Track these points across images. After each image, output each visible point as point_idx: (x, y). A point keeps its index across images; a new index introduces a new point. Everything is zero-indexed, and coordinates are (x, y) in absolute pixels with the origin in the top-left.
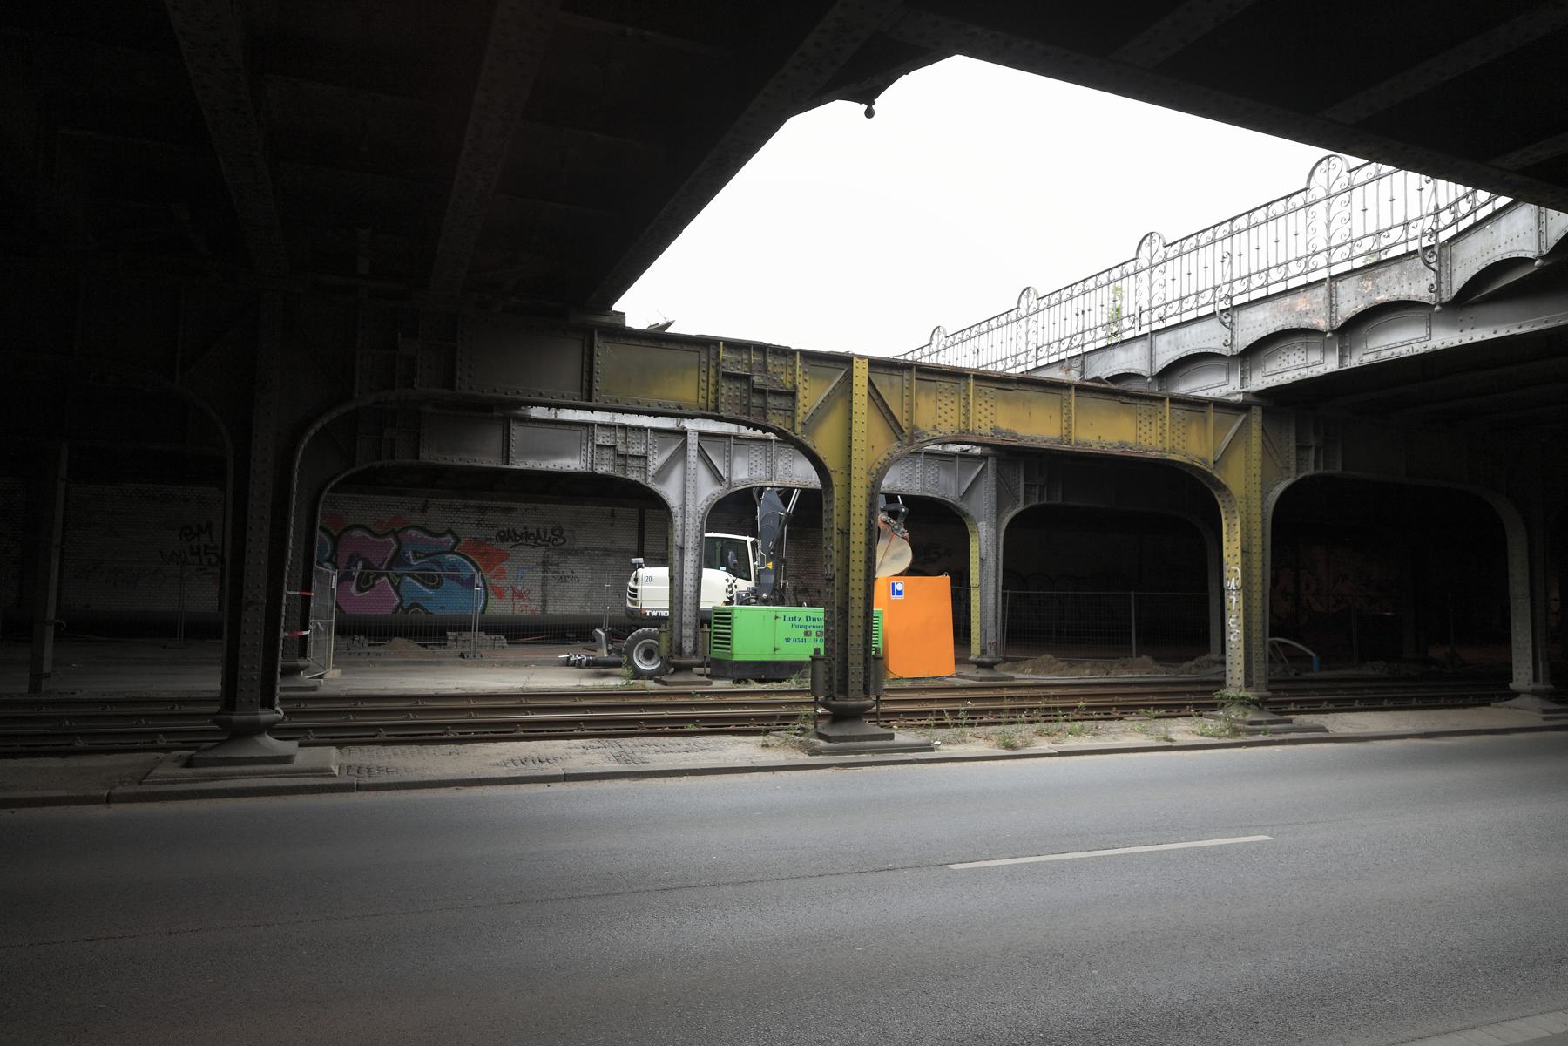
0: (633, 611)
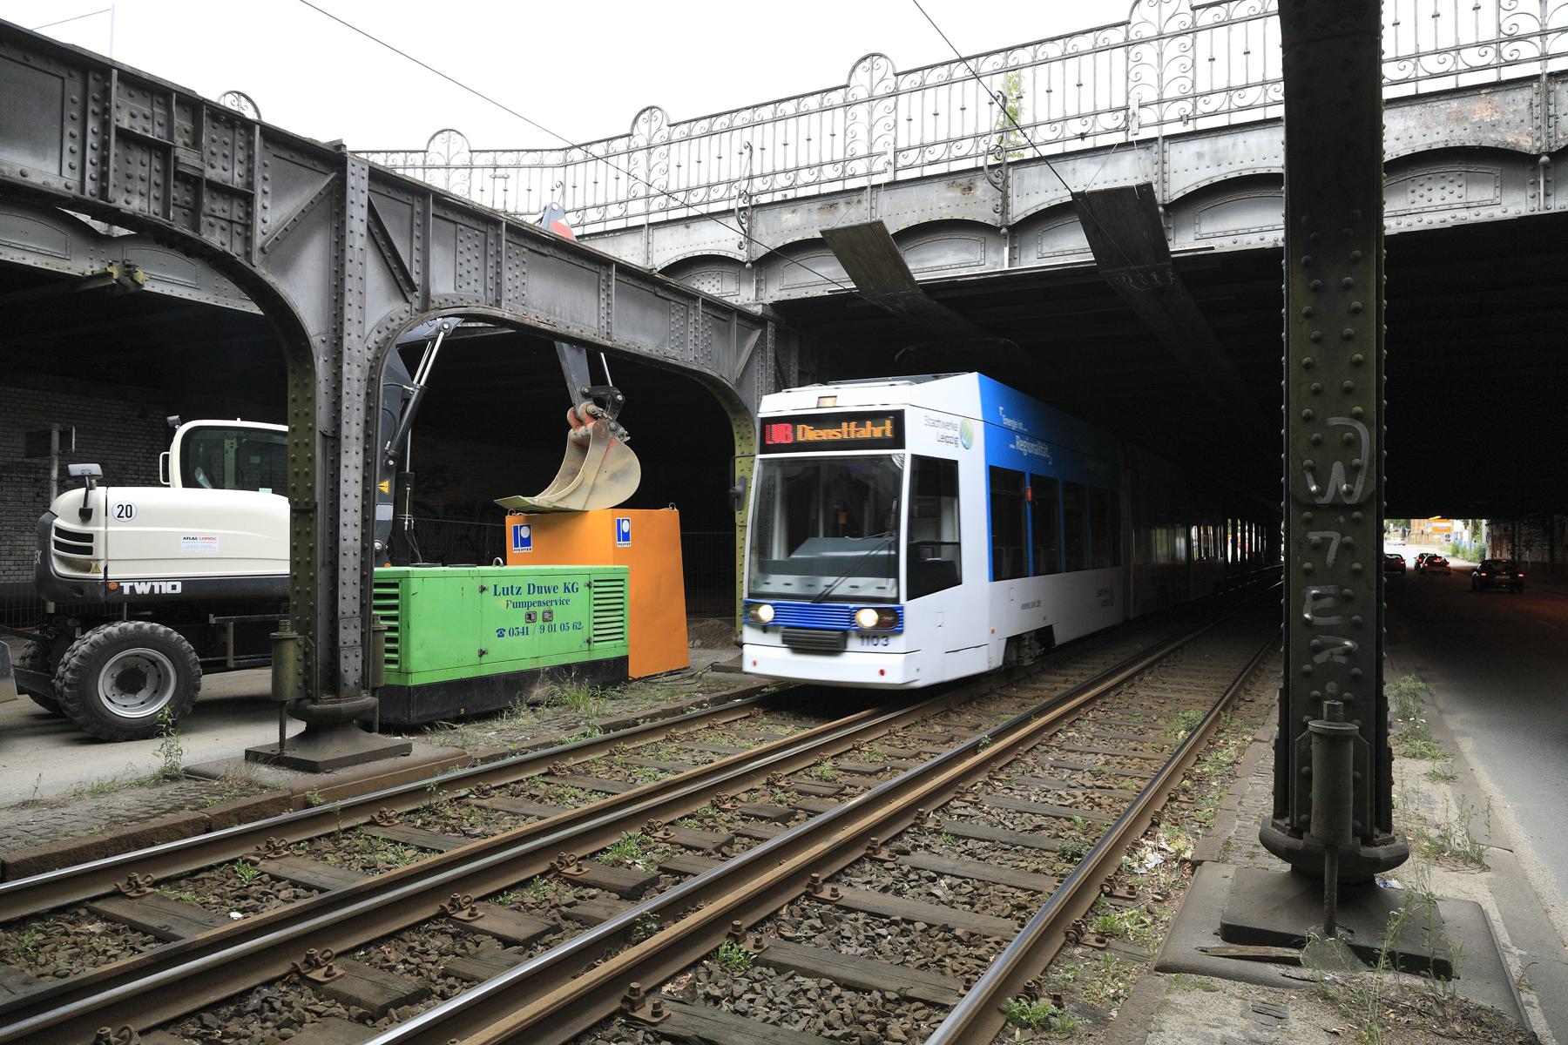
0: (78, 586)
